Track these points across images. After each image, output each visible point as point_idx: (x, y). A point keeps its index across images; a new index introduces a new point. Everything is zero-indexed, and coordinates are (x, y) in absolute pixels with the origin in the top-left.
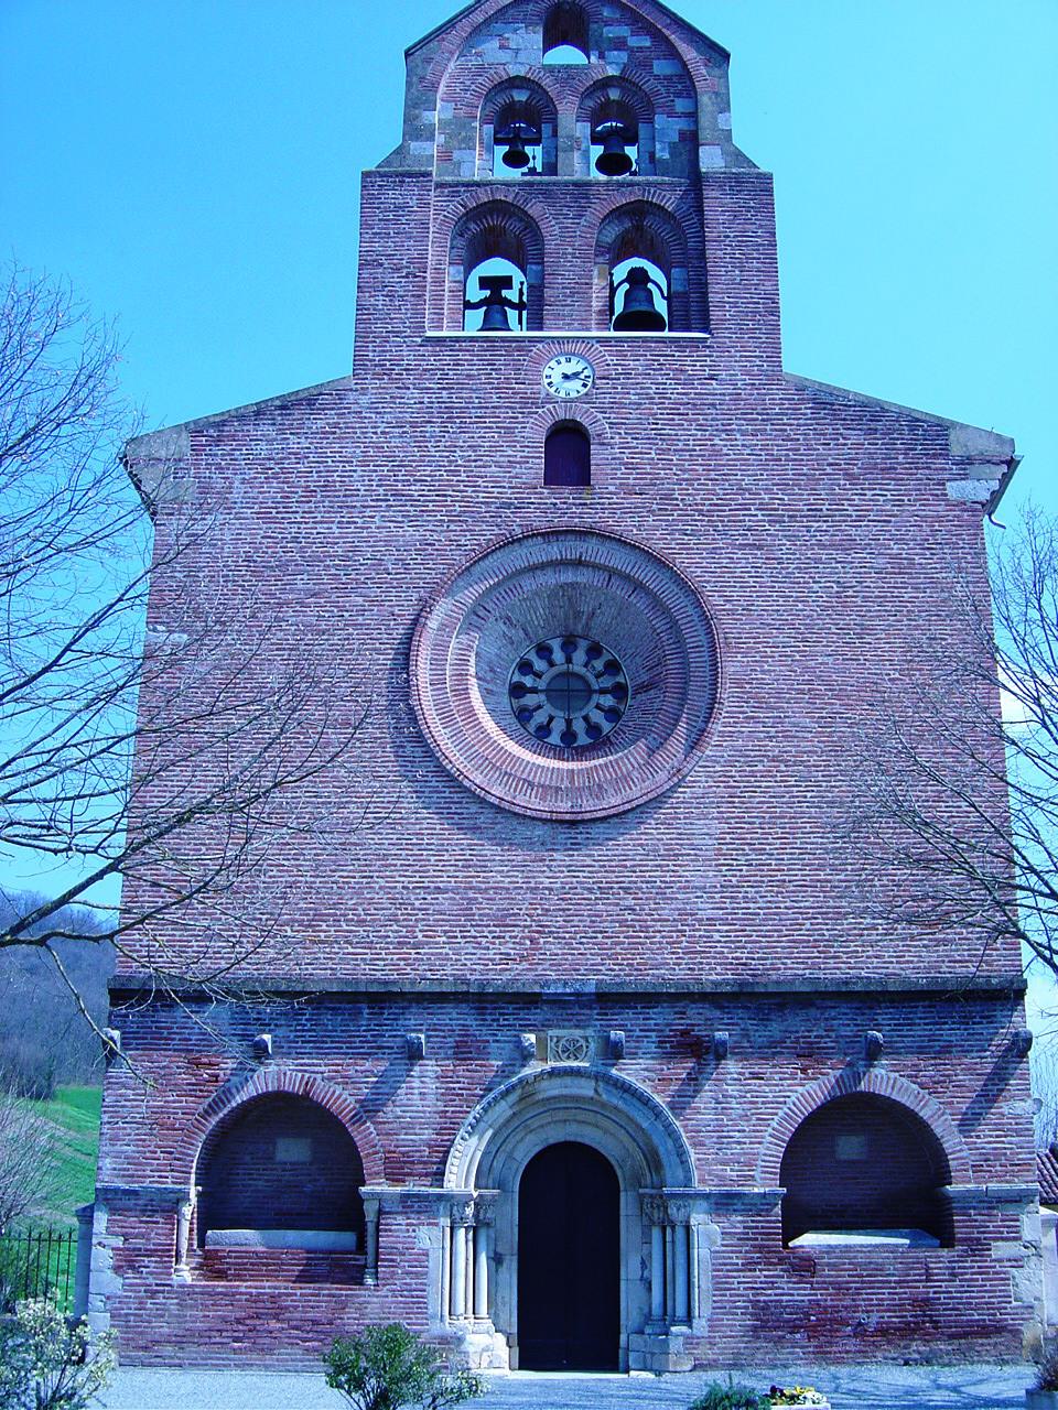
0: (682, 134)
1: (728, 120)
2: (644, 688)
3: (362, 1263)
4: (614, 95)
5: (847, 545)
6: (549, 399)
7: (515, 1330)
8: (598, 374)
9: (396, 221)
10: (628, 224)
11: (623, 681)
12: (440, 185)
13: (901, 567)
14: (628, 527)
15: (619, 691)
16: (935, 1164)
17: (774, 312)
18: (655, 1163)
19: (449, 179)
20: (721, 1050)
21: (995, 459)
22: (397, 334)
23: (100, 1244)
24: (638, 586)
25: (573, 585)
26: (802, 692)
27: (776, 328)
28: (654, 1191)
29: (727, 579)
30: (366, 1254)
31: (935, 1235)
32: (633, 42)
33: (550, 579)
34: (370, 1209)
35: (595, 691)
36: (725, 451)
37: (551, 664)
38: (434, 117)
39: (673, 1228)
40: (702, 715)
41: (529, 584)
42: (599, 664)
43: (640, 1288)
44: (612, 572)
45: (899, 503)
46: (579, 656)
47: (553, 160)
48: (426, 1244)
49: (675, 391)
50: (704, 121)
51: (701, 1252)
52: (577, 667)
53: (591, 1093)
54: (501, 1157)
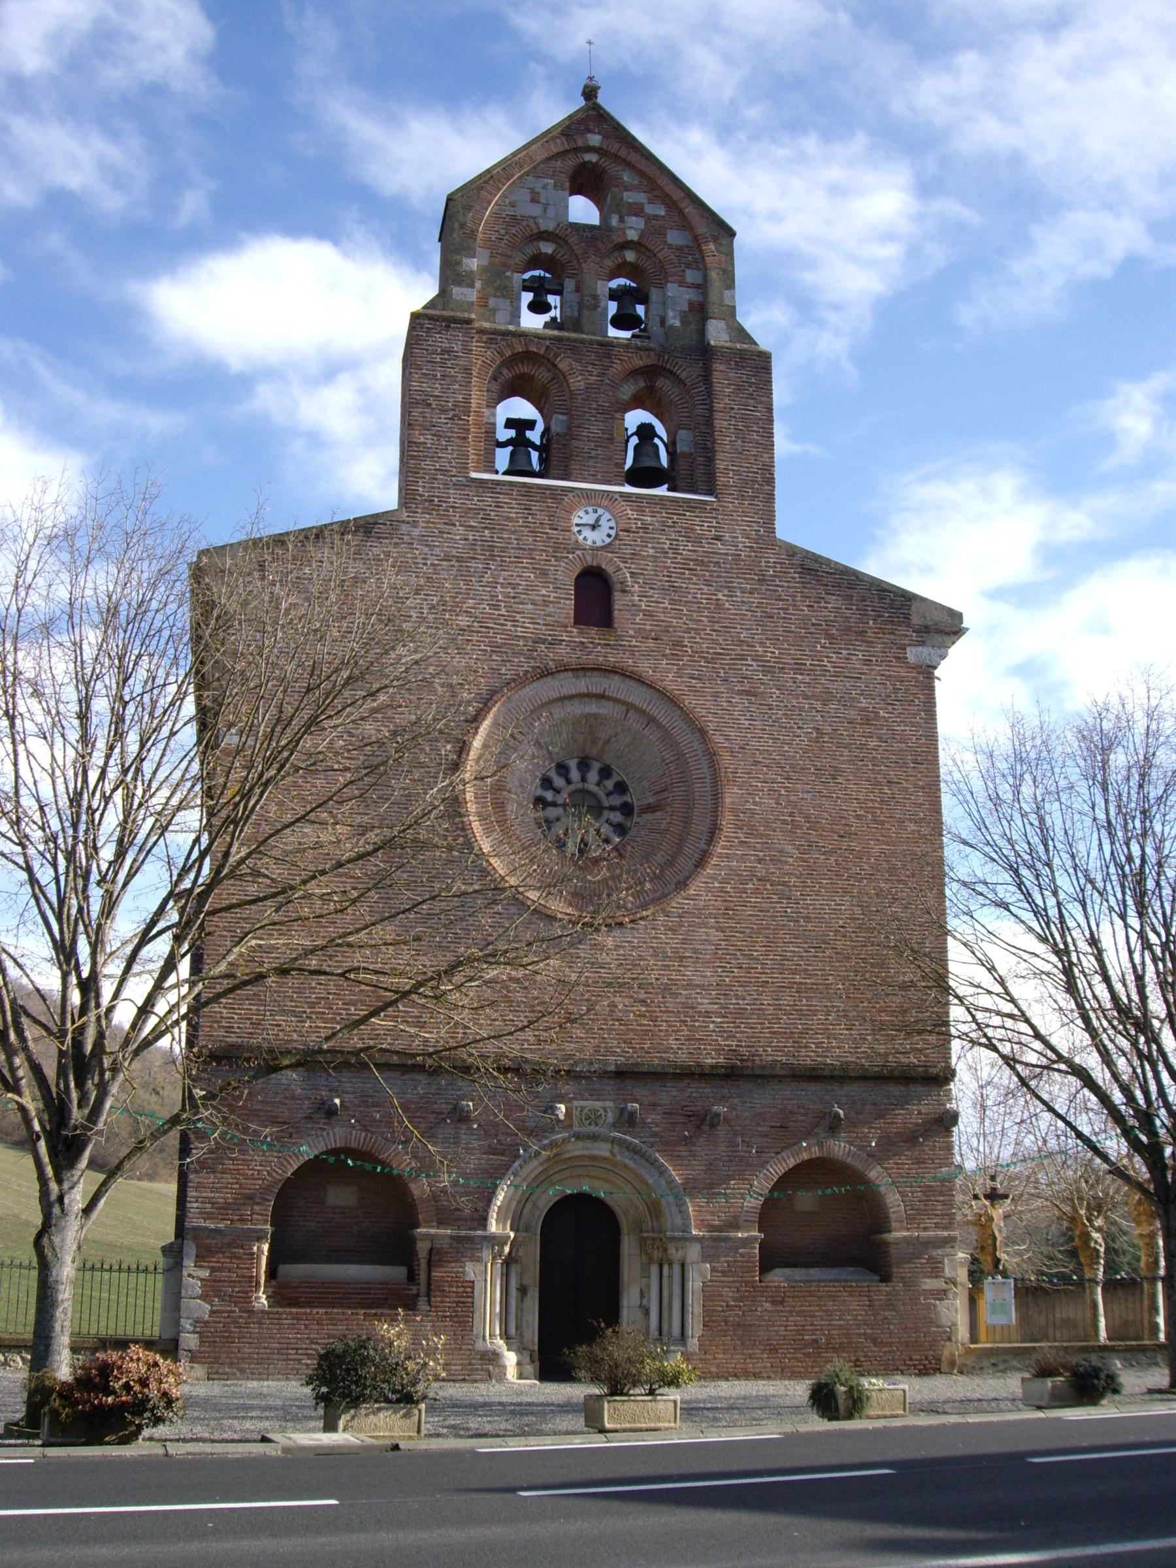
0: (691, 304)
1: (733, 297)
2: (649, 809)
3: (415, 1292)
4: (630, 256)
5: (827, 697)
6: (577, 546)
7: (536, 1348)
8: (621, 526)
9: (443, 364)
10: (642, 384)
11: (629, 800)
12: (481, 332)
13: (869, 718)
14: (645, 668)
15: (627, 809)
16: (877, 1219)
17: (770, 481)
18: (655, 1210)
19: (487, 325)
20: (716, 1121)
21: (947, 630)
22: (444, 472)
23: (189, 1275)
24: (651, 720)
25: (596, 716)
26: (785, 822)
27: (770, 498)
28: (656, 1235)
29: (733, 724)
30: (419, 1284)
31: (874, 1270)
32: (650, 209)
33: (576, 709)
34: (422, 1247)
35: (606, 808)
36: (727, 605)
37: (569, 782)
38: (473, 264)
39: (670, 1264)
40: (705, 837)
41: (559, 712)
42: (610, 784)
43: (638, 1314)
44: (629, 706)
45: (867, 662)
46: (593, 776)
47: (576, 314)
48: (472, 1277)
49: (686, 549)
50: (713, 296)
51: (695, 1283)
52: (591, 786)
53: (608, 1154)
54: (529, 1206)
